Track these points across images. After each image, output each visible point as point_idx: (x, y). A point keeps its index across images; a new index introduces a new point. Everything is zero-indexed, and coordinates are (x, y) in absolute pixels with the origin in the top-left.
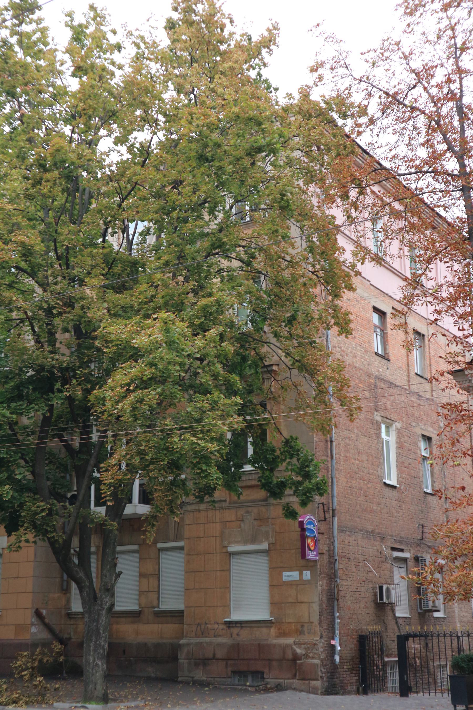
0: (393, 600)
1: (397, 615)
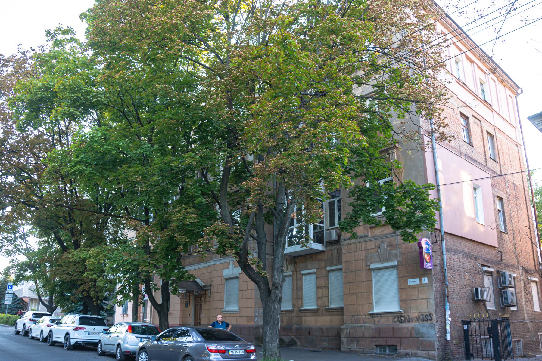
0: (485, 298)
1: (488, 308)
